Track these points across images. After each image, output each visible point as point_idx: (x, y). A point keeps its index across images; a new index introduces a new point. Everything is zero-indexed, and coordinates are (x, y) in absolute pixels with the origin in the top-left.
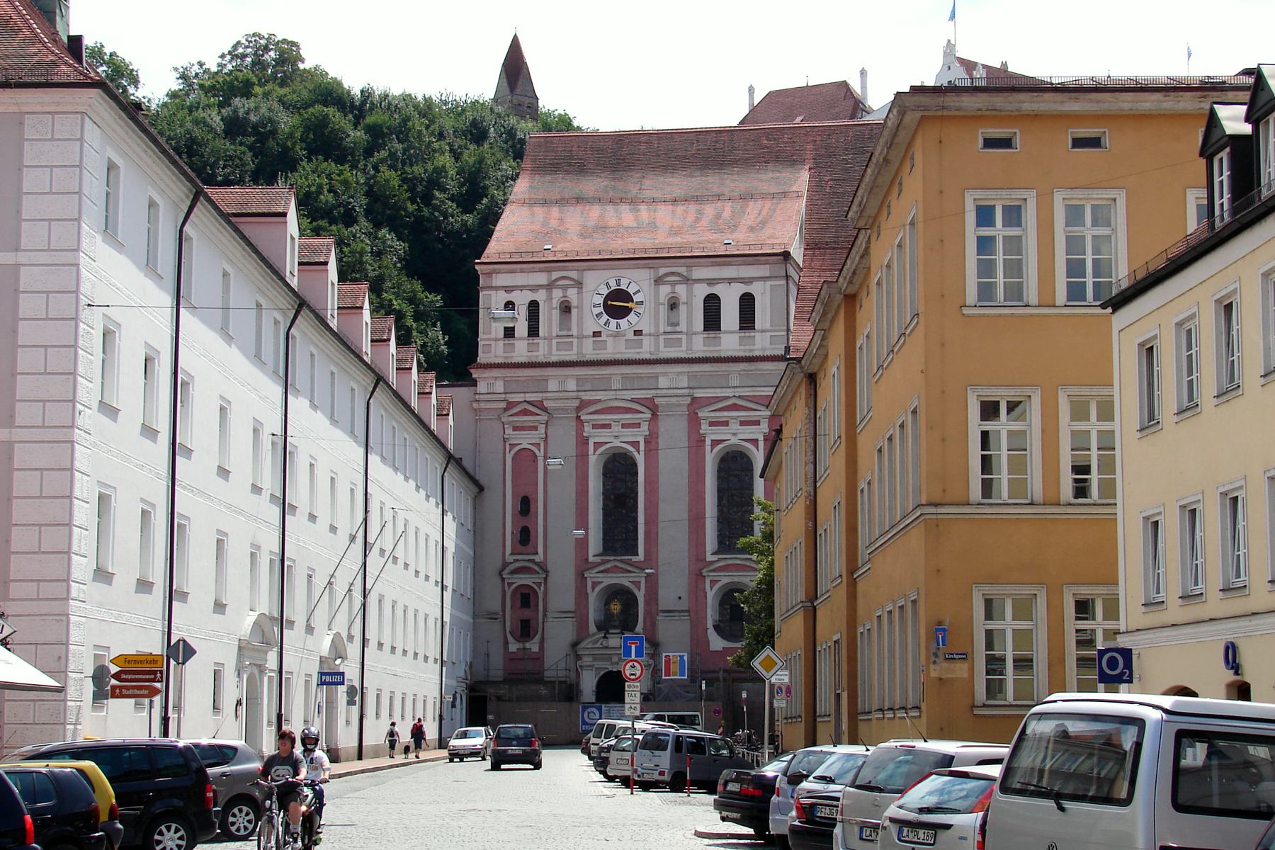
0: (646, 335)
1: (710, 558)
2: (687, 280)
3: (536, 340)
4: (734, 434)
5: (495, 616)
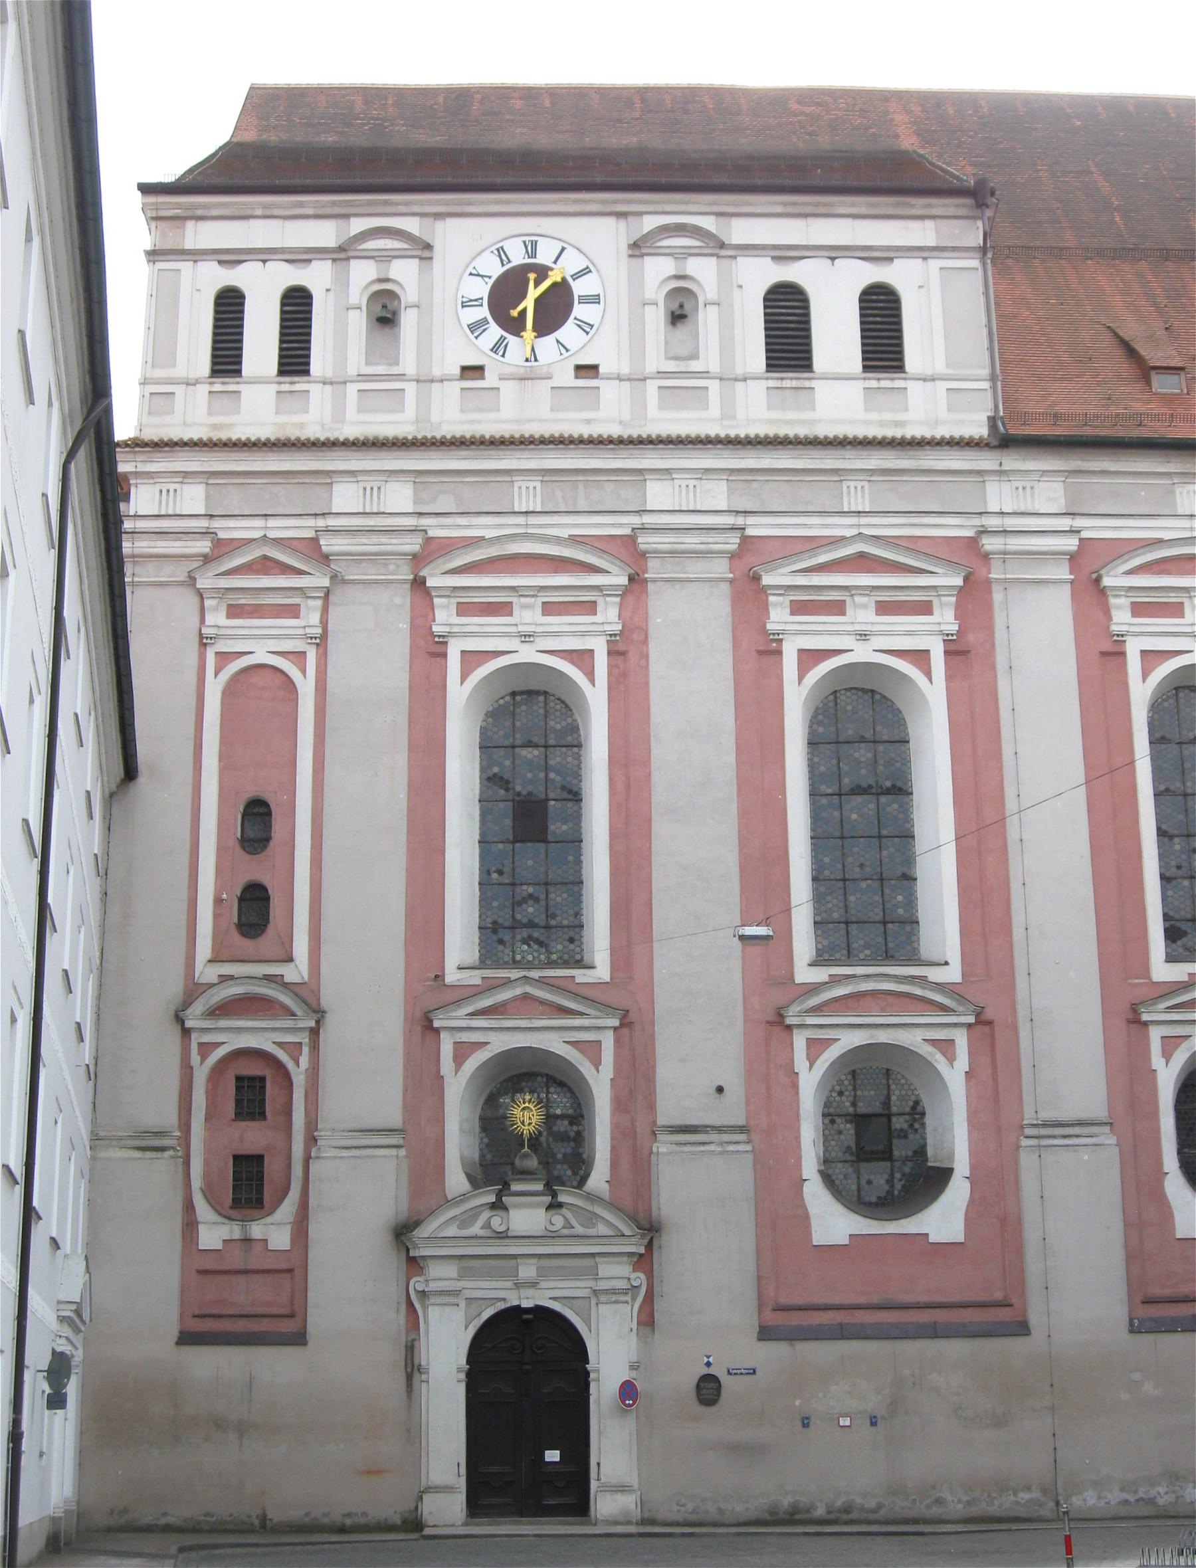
0: (609, 378)
1: (804, 974)
2: (717, 246)
3: (300, 384)
4: (863, 636)
5: (157, 1142)
